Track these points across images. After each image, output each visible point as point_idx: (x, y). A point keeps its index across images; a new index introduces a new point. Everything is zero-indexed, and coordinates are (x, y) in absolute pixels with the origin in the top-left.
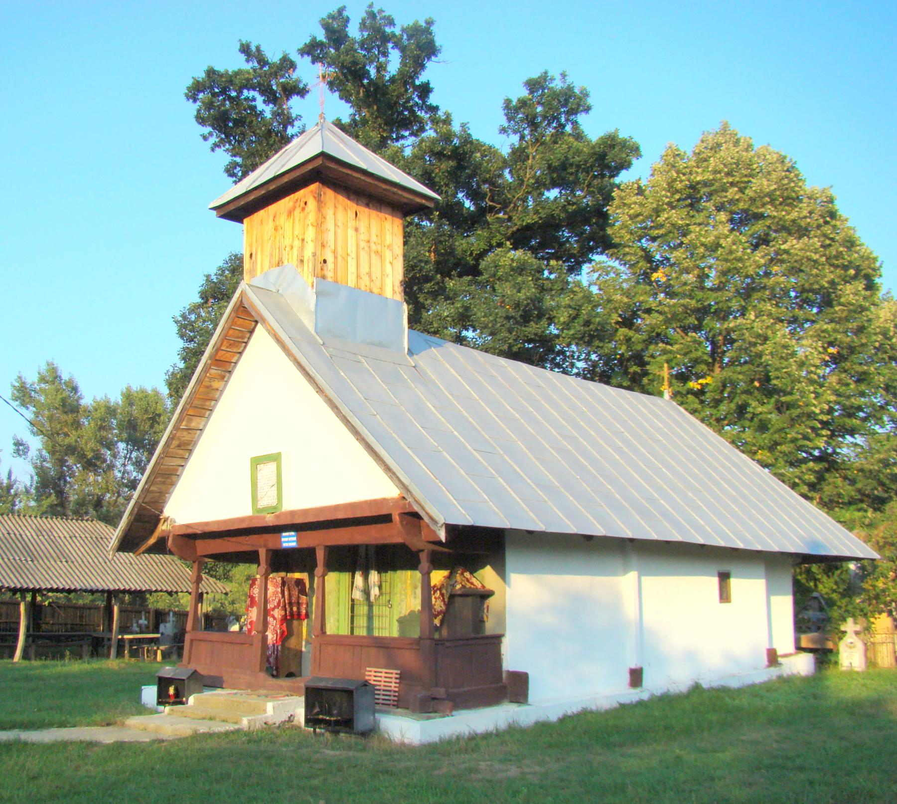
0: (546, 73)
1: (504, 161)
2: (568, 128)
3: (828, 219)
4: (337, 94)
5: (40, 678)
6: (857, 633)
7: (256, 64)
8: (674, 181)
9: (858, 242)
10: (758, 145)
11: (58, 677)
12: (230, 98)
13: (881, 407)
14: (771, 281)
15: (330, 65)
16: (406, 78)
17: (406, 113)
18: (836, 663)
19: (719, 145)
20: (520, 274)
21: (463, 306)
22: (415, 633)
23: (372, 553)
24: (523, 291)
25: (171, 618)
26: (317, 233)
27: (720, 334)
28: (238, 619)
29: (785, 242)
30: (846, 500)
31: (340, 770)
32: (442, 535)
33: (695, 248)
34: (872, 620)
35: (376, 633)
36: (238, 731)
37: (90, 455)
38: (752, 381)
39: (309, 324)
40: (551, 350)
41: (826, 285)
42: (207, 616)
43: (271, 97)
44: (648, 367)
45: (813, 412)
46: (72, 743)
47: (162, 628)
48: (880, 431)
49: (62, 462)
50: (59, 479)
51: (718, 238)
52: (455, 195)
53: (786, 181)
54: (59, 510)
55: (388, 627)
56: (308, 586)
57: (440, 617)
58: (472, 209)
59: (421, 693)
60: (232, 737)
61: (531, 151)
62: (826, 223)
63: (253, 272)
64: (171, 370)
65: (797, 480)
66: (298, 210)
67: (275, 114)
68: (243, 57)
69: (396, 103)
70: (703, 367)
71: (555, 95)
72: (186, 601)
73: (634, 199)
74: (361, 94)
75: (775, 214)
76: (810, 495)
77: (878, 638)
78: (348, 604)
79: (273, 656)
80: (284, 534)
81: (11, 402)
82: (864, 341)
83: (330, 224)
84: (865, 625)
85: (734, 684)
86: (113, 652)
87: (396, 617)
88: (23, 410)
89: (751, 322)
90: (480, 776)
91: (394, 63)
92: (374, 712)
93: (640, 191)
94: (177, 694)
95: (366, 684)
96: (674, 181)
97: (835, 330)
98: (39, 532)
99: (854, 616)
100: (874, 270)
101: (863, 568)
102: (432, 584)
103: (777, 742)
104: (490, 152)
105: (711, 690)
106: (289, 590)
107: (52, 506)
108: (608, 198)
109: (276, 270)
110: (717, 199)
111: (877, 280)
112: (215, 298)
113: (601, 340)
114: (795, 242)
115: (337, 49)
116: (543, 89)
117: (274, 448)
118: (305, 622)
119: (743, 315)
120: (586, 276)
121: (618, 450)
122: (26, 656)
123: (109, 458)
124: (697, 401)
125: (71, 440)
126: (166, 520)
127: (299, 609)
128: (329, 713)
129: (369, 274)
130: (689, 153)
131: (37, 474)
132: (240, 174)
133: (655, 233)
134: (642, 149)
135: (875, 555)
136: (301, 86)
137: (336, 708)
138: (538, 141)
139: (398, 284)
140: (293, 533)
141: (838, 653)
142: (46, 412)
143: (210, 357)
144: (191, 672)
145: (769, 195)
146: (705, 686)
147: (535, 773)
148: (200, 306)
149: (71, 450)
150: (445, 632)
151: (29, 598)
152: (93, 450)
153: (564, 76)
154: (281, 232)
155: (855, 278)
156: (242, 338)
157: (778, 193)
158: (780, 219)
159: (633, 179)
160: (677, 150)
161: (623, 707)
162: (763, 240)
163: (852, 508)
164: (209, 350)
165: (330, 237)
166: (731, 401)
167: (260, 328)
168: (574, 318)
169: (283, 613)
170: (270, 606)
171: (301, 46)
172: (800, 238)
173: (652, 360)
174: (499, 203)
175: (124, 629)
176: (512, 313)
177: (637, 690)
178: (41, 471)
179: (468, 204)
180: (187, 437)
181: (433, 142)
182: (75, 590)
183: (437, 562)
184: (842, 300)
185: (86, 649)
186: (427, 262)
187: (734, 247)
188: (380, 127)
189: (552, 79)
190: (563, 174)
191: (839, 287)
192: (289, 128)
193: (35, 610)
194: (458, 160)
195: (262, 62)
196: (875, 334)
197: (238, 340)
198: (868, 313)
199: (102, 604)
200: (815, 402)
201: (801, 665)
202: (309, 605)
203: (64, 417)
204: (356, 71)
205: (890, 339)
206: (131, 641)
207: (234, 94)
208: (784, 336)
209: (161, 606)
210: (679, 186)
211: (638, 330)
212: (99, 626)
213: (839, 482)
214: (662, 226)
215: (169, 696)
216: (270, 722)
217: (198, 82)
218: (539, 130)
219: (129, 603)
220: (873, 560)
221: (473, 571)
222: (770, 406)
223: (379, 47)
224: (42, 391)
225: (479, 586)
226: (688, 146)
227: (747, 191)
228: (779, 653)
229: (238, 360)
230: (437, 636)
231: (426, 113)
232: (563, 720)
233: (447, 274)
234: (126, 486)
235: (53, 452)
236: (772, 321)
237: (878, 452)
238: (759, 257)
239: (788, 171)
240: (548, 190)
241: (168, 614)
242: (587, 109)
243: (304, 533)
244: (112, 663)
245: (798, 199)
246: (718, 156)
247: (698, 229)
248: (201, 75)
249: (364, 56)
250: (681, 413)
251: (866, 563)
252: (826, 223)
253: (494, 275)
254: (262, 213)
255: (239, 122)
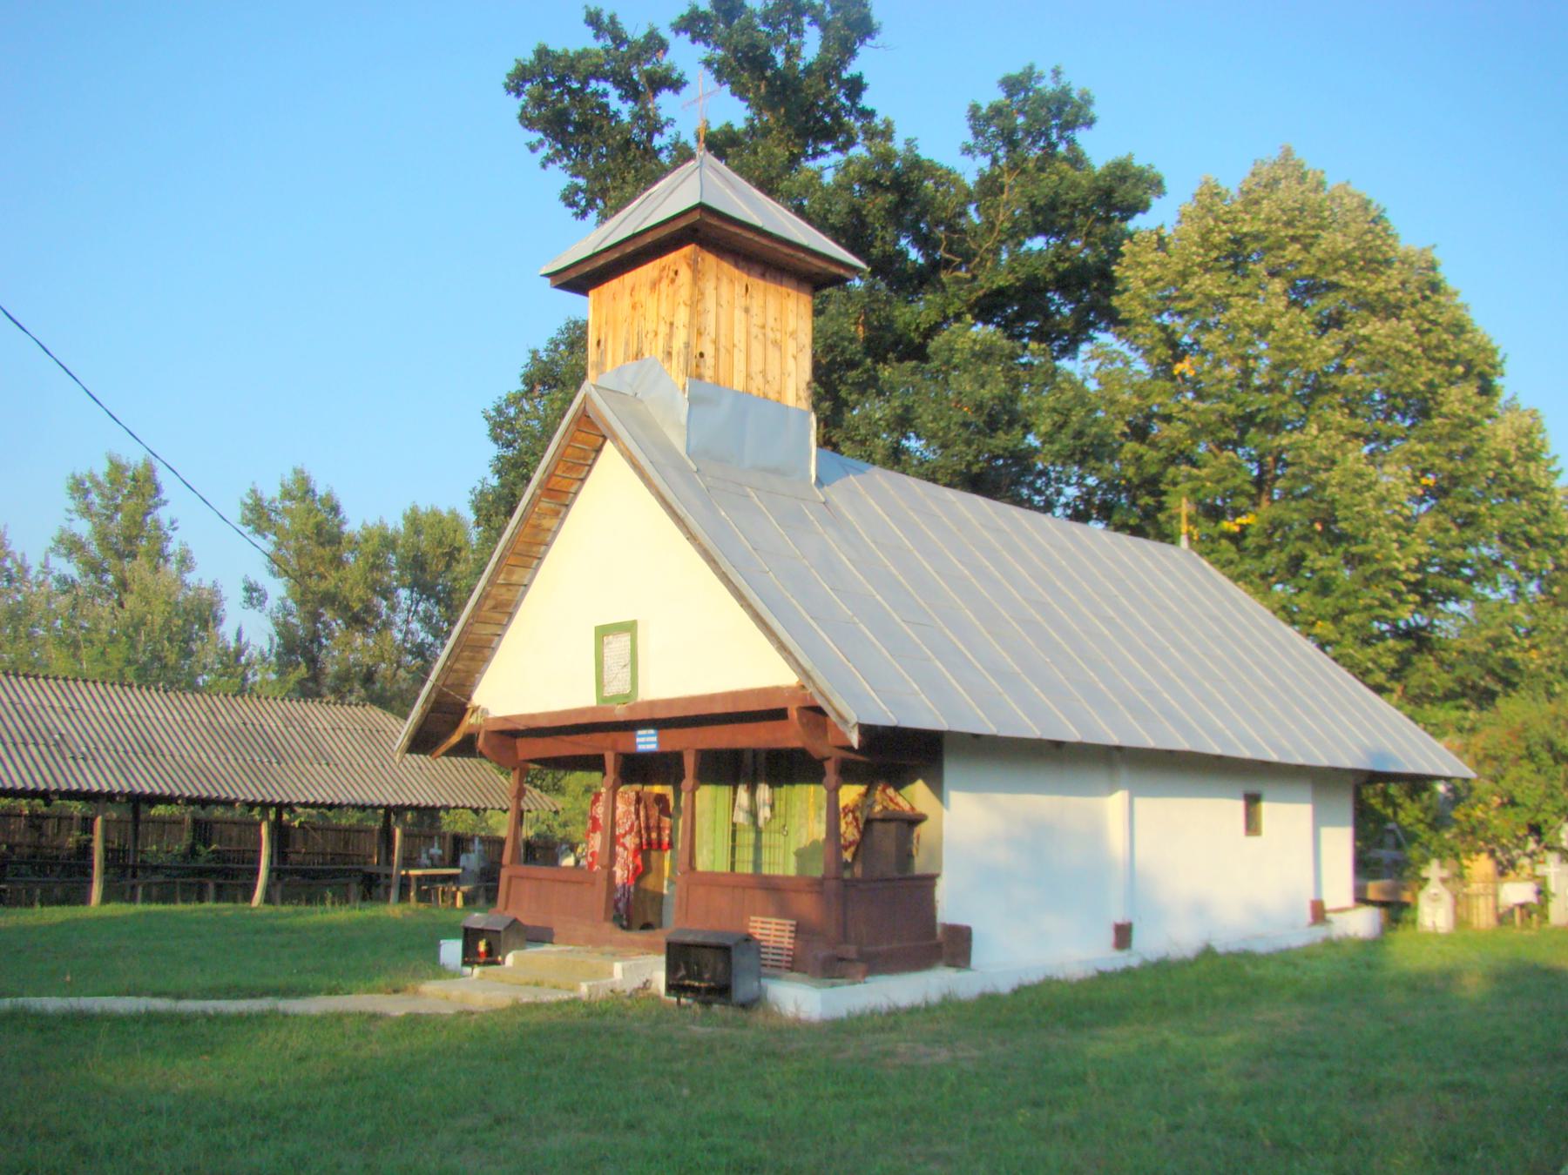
0: (1031, 68)
1: (969, 194)
2: (1062, 148)
3: (1428, 293)
4: (727, 88)
5: (292, 930)
6: (1444, 881)
7: (609, 42)
8: (1210, 231)
9: (1469, 327)
10: (1332, 182)
11: (319, 928)
12: (571, 92)
13: (1496, 563)
14: (1342, 381)
15: (717, 46)
16: (829, 69)
17: (827, 120)
18: (1414, 922)
19: (1276, 181)
20: (985, 362)
21: (902, 405)
22: (817, 870)
23: (762, 758)
24: (988, 387)
25: (477, 846)
26: (692, 316)
27: (1270, 453)
28: (573, 848)
29: (1364, 325)
30: (1440, 693)
31: (711, 1050)
32: (854, 739)
33: (1237, 329)
34: (1465, 862)
35: (766, 870)
36: (574, 1001)
37: (357, 607)
38: (1313, 522)
39: (678, 442)
40: (1028, 469)
41: (1422, 388)
42: (529, 845)
43: (631, 91)
44: (1164, 498)
45: (1396, 570)
46: (348, 1015)
47: (463, 859)
48: (1493, 596)
49: (315, 617)
50: (312, 642)
51: (1270, 316)
52: (896, 242)
53: (1369, 237)
54: (310, 689)
55: (781, 863)
56: (672, 803)
57: (852, 849)
58: (921, 261)
59: (823, 952)
60: (566, 1009)
61: (1007, 180)
62: (1425, 298)
63: (600, 366)
64: (479, 487)
65: (1370, 665)
66: (665, 283)
67: (637, 117)
68: (590, 31)
69: (813, 104)
70: (1242, 502)
71: (1043, 101)
72: (501, 825)
73: (1152, 256)
74: (763, 90)
75: (1352, 283)
76: (1388, 685)
77: (1474, 887)
78: (728, 829)
79: (624, 900)
80: (640, 732)
81: (242, 528)
82: (1473, 468)
83: (710, 303)
84: (1456, 870)
85: (1260, 947)
86: (394, 894)
87: (793, 849)
88: (258, 540)
89: (1310, 438)
90: (897, 1061)
91: (811, 46)
92: (760, 976)
93: (1162, 244)
94: (490, 951)
95: (748, 939)
96: (1210, 231)
97: (1431, 453)
98: (288, 721)
99: (1440, 857)
100: (1493, 366)
101: (1454, 790)
102: (842, 804)
103: (1301, 1023)
104: (946, 178)
105: (1229, 954)
106: (646, 807)
107: (301, 682)
108: (1116, 254)
109: (633, 365)
110: (1271, 259)
111: (1498, 381)
112: (544, 384)
113: (1099, 459)
114: (1378, 325)
115: (728, 25)
116: (1027, 90)
117: (625, 610)
118: (668, 854)
119: (1301, 429)
120: (1080, 367)
121: (1107, 620)
122: (268, 899)
123: (384, 611)
124: (1233, 548)
125: (329, 585)
126: (475, 710)
127: (659, 835)
128: (699, 978)
129: (764, 372)
130: (1234, 192)
131: (279, 634)
132: (583, 203)
133: (1182, 305)
134: (1166, 183)
135: (1470, 773)
136: (675, 76)
137: (709, 970)
138: (1016, 167)
139: (803, 386)
140: (652, 732)
141: (1416, 909)
142: (292, 543)
143: (540, 485)
144: (508, 922)
145: (1346, 256)
146: (1220, 949)
147: (972, 1059)
148: (525, 395)
149: (329, 599)
150: (858, 870)
151: (272, 816)
152: (361, 600)
153: (1056, 73)
154: (641, 311)
155: (1465, 376)
156: (585, 458)
157: (1357, 254)
158: (1360, 292)
159: (1153, 227)
160: (1217, 186)
161: (1103, 977)
162: (1334, 321)
163: (1449, 704)
164: (537, 477)
165: (710, 321)
166: (1281, 551)
167: (609, 446)
168: (1060, 427)
169: (637, 840)
170: (619, 831)
171: (675, 18)
172: (1387, 318)
173: (1171, 489)
174: (960, 255)
175: (409, 862)
176: (971, 417)
177: (1124, 953)
178: (285, 630)
179: (914, 254)
180: (505, 595)
181: (866, 165)
182: (340, 806)
183: (849, 773)
184: (1444, 409)
185: (355, 889)
186: (852, 340)
187: (1292, 331)
188: (789, 139)
189: (1040, 77)
190: (1053, 216)
191: (1441, 391)
192: (657, 137)
193: (281, 834)
194: (904, 189)
195: (619, 38)
196: (1489, 459)
197: (579, 464)
198: (1479, 429)
199: (377, 825)
200: (1397, 554)
201: (1361, 923)
202: (673, 830)
203: (319, 551)
204: (755, 58)
205: (1509, 466)
206: (419, 878)
207: (576, 86)
208: (1358, 460)
209: (460, 828)
210: (1217, 239)
211: (1154, 445)
212: (371, 856)
213: (1432, 667)
214: (1189, 297)
215: (478, 954)
216: (618, 989)
217: (524, 67)
218: (1019, 150)
219: (414, 824)
220: (1466, 780)
221: (898, 788)
222: (1337, 559)
223: (789, 22)
224: (288, 512)
225: (906, 807)
226: (1232, 181)
227: (1313, 250)
228: (1328, 905)
229: (580, 489)
230: (847, 875)
231: (857, 119)
232: (1018, 991)
233: (881, 358)
234: (410, 652)
235: (301, 603)
236: (1342, 437)
237: (1487, 627)
238: (1329, 345)
239: (1373, 221)
240: (1030, 237)
241: (472, 839)
242: (1090, 123)
243: (665, 731)
244: (393, 910)
245: (1388, 263)
246: (1274, 197)
247: (1241, 303)
248: (528, 57)
249: (768, 35)
250: (1204, 568)
251: (1459, 783)
252: (1425, 298)
253: (947, 362)
254: (614, 284)
255: (584, 127)
